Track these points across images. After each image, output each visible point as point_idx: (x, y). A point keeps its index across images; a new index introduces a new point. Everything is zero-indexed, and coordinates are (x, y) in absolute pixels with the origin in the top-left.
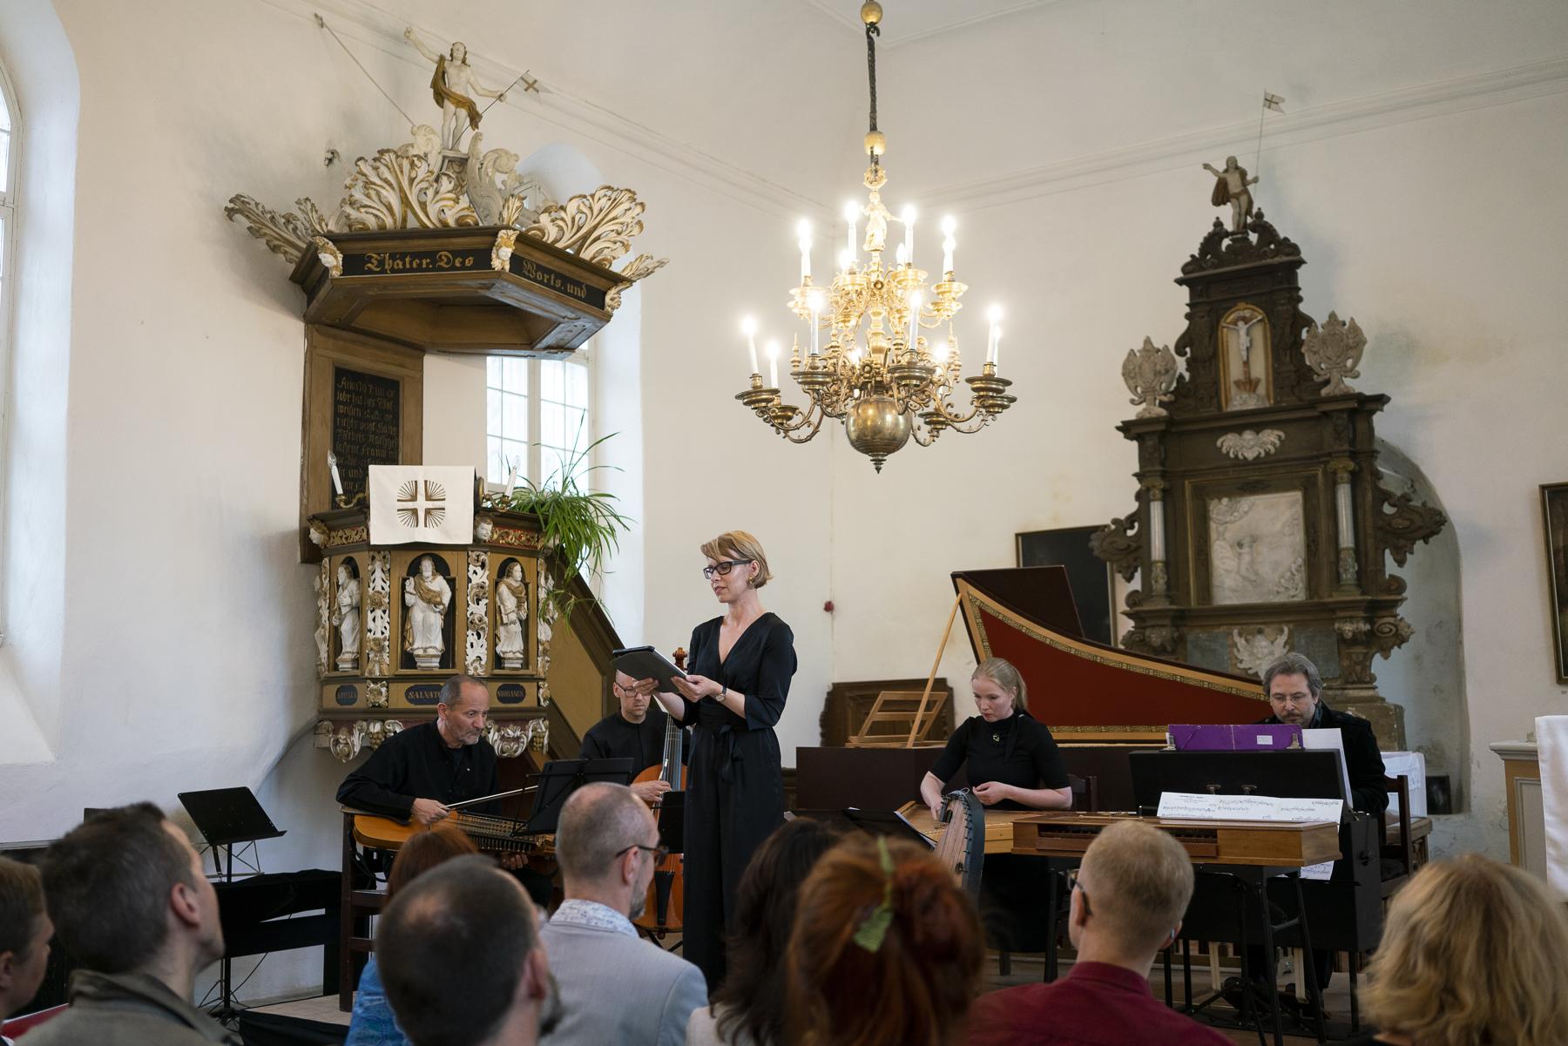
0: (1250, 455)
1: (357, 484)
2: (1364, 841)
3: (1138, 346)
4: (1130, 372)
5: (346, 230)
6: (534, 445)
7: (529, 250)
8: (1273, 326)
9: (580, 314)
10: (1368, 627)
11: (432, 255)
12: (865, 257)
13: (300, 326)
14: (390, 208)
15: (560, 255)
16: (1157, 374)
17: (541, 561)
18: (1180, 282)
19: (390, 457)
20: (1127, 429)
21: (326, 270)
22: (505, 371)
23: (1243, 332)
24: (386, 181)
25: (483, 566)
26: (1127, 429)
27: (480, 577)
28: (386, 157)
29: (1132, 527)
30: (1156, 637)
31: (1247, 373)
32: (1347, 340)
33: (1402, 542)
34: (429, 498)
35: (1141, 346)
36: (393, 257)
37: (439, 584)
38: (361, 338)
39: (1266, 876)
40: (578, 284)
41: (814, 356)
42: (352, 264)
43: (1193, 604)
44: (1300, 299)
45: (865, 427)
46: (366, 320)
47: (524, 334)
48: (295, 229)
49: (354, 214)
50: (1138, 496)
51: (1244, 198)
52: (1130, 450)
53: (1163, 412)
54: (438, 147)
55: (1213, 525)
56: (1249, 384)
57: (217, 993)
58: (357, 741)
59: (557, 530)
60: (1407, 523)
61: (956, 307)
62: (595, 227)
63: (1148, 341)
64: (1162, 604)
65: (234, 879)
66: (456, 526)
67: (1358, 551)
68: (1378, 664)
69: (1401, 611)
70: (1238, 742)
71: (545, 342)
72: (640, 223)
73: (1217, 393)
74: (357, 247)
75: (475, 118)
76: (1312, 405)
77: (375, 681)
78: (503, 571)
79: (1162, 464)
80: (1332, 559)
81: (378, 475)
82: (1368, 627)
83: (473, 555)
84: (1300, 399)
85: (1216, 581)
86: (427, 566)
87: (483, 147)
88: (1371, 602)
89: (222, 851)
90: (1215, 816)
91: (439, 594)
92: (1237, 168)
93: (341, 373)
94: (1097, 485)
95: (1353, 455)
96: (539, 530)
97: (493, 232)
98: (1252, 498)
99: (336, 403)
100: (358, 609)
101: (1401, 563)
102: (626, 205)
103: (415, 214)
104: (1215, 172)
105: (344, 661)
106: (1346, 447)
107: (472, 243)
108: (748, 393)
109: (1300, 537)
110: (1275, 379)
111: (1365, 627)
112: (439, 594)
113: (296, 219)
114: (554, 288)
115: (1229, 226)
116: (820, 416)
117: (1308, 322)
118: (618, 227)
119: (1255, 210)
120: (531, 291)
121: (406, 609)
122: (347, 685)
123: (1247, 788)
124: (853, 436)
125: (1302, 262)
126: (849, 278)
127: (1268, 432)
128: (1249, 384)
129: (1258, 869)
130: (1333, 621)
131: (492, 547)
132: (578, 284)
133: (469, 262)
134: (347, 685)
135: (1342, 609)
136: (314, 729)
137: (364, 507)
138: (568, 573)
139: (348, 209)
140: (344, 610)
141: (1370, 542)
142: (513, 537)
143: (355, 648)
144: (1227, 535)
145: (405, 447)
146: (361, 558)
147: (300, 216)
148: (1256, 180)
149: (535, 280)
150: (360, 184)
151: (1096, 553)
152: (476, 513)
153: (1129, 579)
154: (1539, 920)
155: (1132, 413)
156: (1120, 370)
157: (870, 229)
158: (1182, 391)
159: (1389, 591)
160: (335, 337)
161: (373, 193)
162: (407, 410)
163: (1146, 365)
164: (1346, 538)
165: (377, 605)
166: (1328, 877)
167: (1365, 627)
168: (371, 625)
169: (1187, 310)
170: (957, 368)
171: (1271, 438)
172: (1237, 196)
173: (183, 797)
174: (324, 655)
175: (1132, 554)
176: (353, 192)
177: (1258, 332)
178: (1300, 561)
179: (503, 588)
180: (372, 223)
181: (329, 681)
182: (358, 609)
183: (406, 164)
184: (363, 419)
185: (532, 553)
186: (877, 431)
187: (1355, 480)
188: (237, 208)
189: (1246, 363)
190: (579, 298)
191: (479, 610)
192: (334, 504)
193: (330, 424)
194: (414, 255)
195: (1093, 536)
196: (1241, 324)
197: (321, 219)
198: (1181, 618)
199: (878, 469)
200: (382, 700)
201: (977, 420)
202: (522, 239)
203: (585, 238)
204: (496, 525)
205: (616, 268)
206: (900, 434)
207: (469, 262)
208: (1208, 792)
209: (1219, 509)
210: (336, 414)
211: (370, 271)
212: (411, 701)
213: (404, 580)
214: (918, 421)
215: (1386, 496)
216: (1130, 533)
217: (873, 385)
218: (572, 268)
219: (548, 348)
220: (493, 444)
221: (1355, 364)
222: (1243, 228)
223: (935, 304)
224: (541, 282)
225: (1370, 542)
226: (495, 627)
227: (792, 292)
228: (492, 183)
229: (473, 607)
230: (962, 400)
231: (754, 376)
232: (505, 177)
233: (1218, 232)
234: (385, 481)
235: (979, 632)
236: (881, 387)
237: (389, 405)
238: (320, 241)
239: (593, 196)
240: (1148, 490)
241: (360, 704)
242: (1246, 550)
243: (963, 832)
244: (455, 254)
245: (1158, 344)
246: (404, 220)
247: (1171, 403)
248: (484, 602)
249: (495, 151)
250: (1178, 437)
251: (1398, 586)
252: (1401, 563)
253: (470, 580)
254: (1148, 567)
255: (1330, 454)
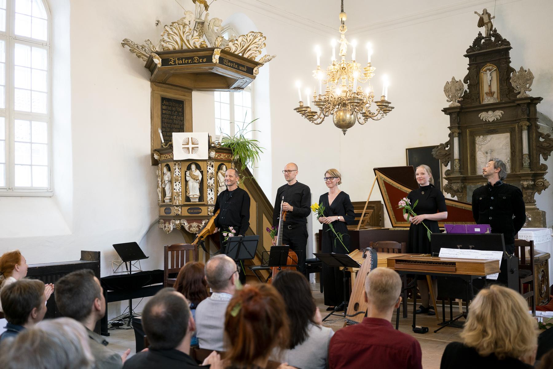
0: (491, 120)
1: (168, 139)
2: (513, 265)
3: (450, 80)
4: (447, 90)
5: (162, 50)
6: (232, 123)
7: (225, 55)
8: (500, 72)
9: (244, 77)
10: (533, 183)
11: (192, 58)
12: (339, 58)
13: (149, 83)
14: (177, 43)
15: (237, 56)
16: (457, 90)
17: (233, 164)
18: (465, 56)
19: (181, 129)
20: (445, 111)
21: (156, 64)
22: (220, 96)
23: (489, 74)
24: (175, 33)
25: (212, 166)
26: (445, 111)
27: (212, 170)
28: (175, 24)
29: (447, 147)
30: (455, 187)
31: (490, 90)
32: (527, 77)
33: (546, 152)
34: (193, 144)
35: (451, 80)
36: (178, 59)
37: (197, 173)
38: (170, 86)
39: (472, 278)
40: (243, 66)
41: (320, 95)
42: (165, 62)
43: (469, 175)
44: (510, 62)
45: (340, 119)
46: (171, 80)
47: (226, 83)
48: (145, 50)
49: (165, 45)
50: (450, 135)
51: (489, 25)
52: (446, 119)
53: (459, 105)
54: (194, 19)
55: (477, 146)
56: (491, 94)
57: (128, 310)
58: (172, 227)
59: (238, 153)
60: (548, 145)
61: (372, 75)
62: (249, 46)
63: (453, 78)
64: (458, 175)
65: (132, 273)
66: (202, 153)
67: (530, 155)
68: (537, 196)
69: (546, 177)
70: (468, 231)
71: (233, 86)
72: (264, 44)
73: (479, 97)
74: (166, 56)
75: (207, 7)
76: (514, 102)
77: (177, 206)
78: (220, 168)
79: (458, 124)
80: (521, 158)
81: (175, 135)
82: (533, 183)
83: (209, 163)
84: (510, 99)
85: (478, 166)
86: (193, 167)
87: (210, 18)
88: (534, 173)
89: (128, 263)
90: (459, 257)
91: (198, 176)
92: (487, 13)
93: (163, 99)
94: (436, 131)
95: (529, 120)
96: (232, 153)
97: (212, 50)
98: (492, 136)
99: (162, 109)
100: (171, 182)
101: (546, 159)
102: (259, 38)
103: (185, 44)
104: (479, 15)
105: (167, 199)
106: (526, 117)
107: (206, 54)
108: (298, 108)
109: (508, 150)
110: (500, 92)
111: (531, 183)
112: (198, 176)
113: (145, 47)
114: (235, 68)
115: (484, 35)
116: (338, 105)
117: (513, 70)
118: (257, 46)
119: (493, 29)
120: (226, 69)
121: (186, 182)
122: (168, 208)
123: (471, 247)
124: (336, 122)
125: (511, 48)
126: (332, 67)
127: (498, 111)
128: (491, 94)
129: (470, 276)
130: (520, 180)
131: (216, 160)
132: (243, 66)
133: (205, 60)
134: (168, 208)
135: (523, 176)
136: (158, 222)
137: (171, 146)
138: (242, 168)
139: (163, 43)
140: (166, 182)
141: (535, 152)
142: (223, 156)
143: (170, 195)
144: (482, 149)
145: (186, 125)
146: (171, 164)
147: (147, 46)
148: (494, 17)
149: (228, 66)
150: (166, 34)
151: (434, 156)
152: (209, 148)
153: (446, 166)
154: (510, 303)
155: (447, 105)
156: (443, 89)
157: (341, 48)
158: (466, 97)
159: (541, 170)
160: (161, 87)
161: (171, 37)
162: (187, 111)
163: (453, 87)
164: (526, 150)
165: (177, 180)
166: (496, 278)
167: (531, 183)
168: (175, 187)
169: (468, 66)
170: (373, 97)
171: (498, 114)
172: (487, 24)
173: (114, 246)
174: (160, 197)
175: (448, 157)
176: (164, 37)
177: (494, 75)
178: (509, 159)
179: (219, 174)
180: (171, 48)
181: (162, 206)
182: (171, 182)
183: (181, 27)
184: (172, 116)
185: (229, 161)
186: (344, 120)
187: (529, 129)
188: (125, 43)
189: (490, 86)
190: (244, 71)
191: (211, 182)
192: (162, 147)
193: (160, 117)
194: (186, 58)
195: (433, 150)
196: (488, 71)
197: (154, 47)
198: (465, 180)
199: (344, 134)
200: (179, 213)
201: (379, 116)
202: (223, 51)
203: (245, 50)
204: (216, 152)
205: (257, 60)
206: (352, 122)
207: (205, 60)
208: (457, 248)
209: (479, 140)
210: (162, 114)
211: (171, 65)
212: (189, 213)
213: (186, 172)
214: (360, 115)
215: (541, 135)
216: (447, 149)
217: (342, 104)
218: (241, 61)
219: (235, 88)
220: (217, 122)
221: (530, 86)
222: (489, 35)
223: (365, 74)
224: (230, 66)
225: (535, 152)
226: (217, 187)
227: (313, 72)
228: (213, 31)
229: (209, 181)
230: (374, 108)
231: (300, 102)
232: (217, 28)
233: (480, 37)
234: (178, 138)
235: (384, 189)
236: (345, 105)
237: (180, 110)
238: (154, 54)
239: (247, 35)
240: (453, 133)
241: (172, 214)
242: (489, 155)
243: (370, 262)
244: (200, 57)
245: (457, 80)
246: (182, 46)
247: (461, 101)
248: (213, 179)
249: (214, 19)
250: (464, 114)
251: (545, 167)
252: (546, 159)
253: (208, 172)
254: (453, 161)
255: (520, 120)
